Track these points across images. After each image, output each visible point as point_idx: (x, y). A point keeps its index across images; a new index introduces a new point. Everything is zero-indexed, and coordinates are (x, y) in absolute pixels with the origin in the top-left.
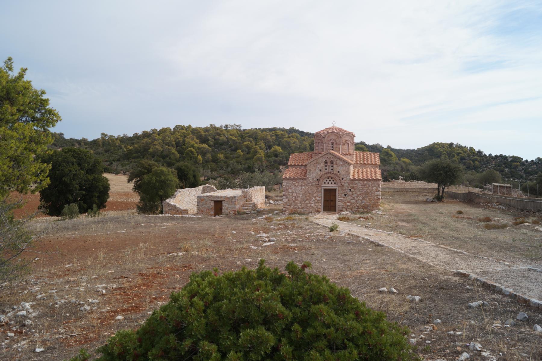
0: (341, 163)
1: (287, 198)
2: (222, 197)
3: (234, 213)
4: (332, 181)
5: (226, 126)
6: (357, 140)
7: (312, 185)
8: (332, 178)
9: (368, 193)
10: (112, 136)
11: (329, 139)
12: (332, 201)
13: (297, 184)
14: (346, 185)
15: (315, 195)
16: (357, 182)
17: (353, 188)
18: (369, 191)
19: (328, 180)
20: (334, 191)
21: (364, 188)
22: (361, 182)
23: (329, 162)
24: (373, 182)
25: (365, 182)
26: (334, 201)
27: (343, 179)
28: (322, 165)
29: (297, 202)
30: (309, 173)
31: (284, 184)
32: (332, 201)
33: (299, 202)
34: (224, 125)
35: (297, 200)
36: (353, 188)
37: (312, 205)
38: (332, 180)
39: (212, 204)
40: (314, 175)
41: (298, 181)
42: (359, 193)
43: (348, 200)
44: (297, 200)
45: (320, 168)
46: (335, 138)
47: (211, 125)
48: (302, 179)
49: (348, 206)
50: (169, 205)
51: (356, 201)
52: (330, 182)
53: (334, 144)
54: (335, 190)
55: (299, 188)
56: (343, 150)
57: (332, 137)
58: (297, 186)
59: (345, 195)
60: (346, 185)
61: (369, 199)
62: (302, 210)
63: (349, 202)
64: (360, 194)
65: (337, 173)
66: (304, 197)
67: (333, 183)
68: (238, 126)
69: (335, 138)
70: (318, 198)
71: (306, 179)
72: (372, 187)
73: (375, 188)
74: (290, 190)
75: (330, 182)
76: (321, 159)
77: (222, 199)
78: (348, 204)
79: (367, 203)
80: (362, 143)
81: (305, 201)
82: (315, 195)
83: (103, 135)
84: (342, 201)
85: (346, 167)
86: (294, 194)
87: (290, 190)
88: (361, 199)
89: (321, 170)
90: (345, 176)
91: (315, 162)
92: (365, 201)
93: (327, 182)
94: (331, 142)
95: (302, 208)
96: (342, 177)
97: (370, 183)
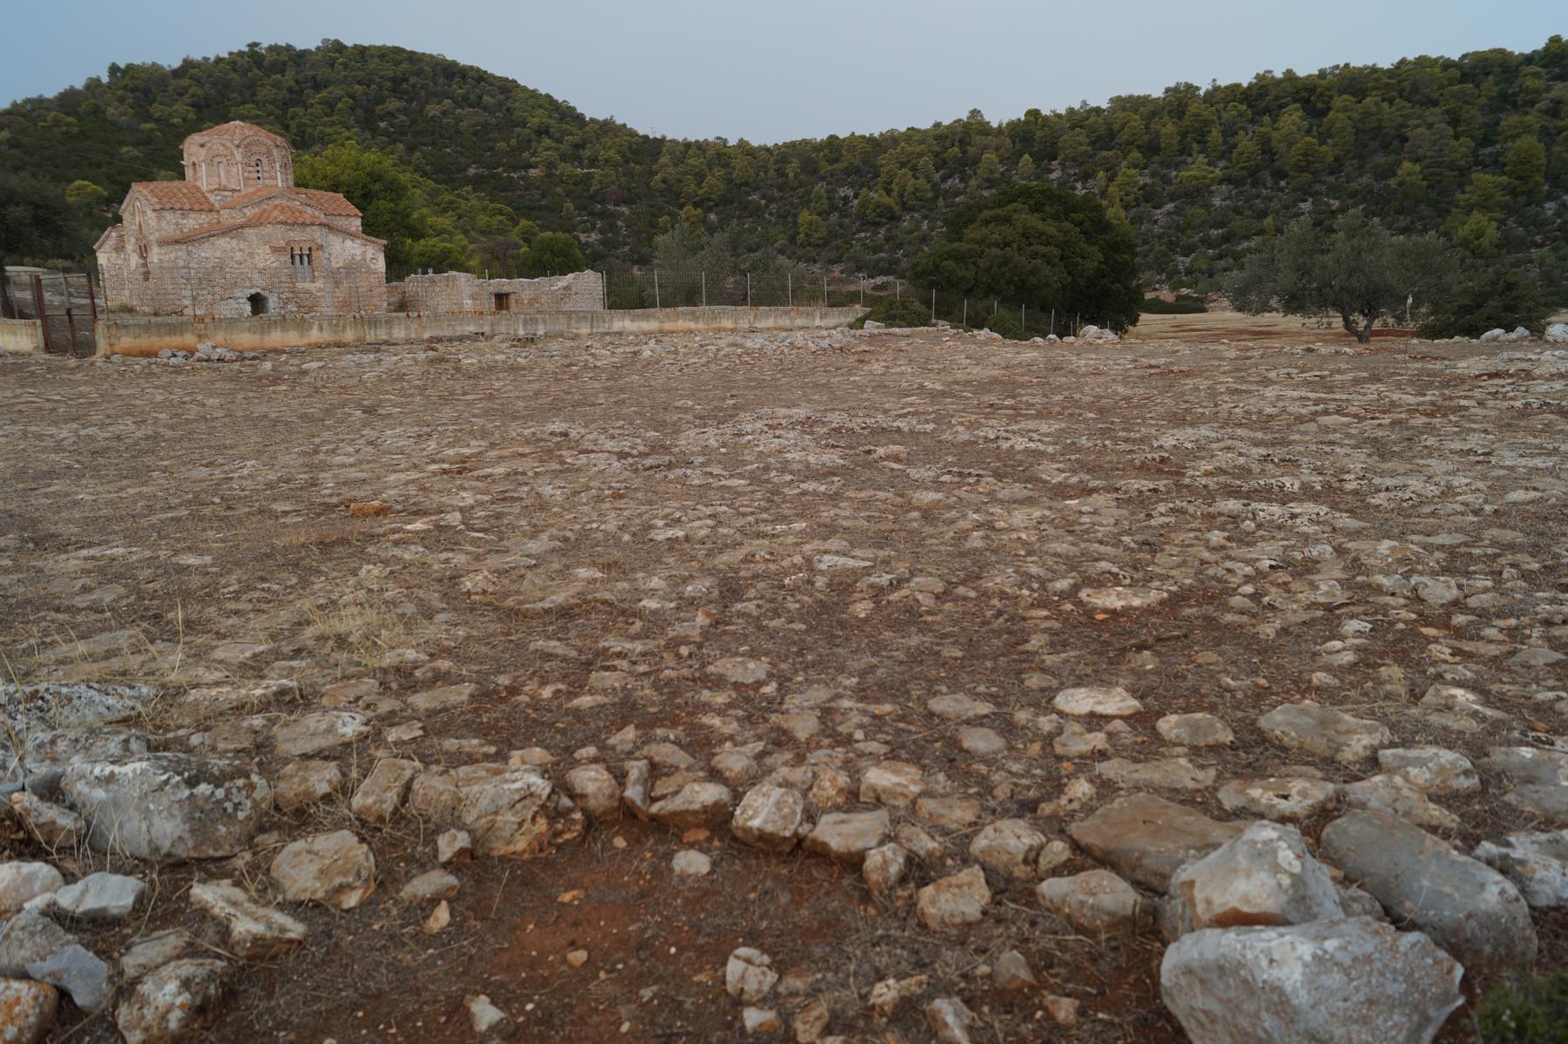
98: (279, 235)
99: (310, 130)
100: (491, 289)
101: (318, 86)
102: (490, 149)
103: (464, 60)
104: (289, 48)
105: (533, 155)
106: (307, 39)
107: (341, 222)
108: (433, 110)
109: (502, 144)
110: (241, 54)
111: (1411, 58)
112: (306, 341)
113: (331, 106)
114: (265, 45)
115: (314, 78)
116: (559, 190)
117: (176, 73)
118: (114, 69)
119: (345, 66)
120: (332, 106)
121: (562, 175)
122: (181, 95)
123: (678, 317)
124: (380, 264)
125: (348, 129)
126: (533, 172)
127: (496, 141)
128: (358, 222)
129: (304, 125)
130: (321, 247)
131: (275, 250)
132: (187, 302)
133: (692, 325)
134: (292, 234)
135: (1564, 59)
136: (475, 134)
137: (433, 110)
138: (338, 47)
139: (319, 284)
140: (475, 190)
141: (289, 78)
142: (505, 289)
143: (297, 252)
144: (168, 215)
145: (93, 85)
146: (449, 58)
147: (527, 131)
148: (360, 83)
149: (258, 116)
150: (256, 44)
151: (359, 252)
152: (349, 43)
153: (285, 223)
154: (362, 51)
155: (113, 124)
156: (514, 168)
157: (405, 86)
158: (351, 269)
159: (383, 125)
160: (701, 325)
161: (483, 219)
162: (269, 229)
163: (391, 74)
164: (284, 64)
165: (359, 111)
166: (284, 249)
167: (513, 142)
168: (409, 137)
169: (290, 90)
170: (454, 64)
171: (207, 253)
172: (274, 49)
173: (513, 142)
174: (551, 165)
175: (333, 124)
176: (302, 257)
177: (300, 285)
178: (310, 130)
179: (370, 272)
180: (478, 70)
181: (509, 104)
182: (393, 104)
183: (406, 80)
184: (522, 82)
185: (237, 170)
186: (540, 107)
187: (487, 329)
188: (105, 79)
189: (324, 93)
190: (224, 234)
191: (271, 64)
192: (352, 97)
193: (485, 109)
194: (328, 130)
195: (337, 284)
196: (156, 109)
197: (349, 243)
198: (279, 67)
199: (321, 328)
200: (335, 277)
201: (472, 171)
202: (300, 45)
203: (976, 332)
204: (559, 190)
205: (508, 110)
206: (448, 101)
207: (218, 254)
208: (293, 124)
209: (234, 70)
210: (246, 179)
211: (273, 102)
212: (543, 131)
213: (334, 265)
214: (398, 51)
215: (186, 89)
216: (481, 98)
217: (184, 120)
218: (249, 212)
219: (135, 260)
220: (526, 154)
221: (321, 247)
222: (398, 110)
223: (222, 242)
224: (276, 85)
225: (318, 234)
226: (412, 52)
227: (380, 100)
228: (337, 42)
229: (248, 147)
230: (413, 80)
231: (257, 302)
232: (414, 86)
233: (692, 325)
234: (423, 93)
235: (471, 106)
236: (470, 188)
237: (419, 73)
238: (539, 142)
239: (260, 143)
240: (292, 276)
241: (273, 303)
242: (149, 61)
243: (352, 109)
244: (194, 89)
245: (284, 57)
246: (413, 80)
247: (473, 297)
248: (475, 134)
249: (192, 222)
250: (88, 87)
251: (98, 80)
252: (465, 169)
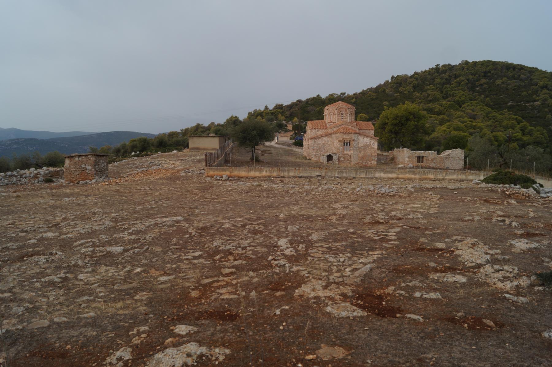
98: (340, 136)
99: (449, 92)
100: (416, 155)
101: (456, 77)
102: (519, 95)
103: (516, 62)
104: (449, 65)
105: (538, 96)
106: (456, 61)
107: (367, 132)
108: (498, 82)
109: (525, 93)
110: (433, 68)
111: (304, 99)
112: (261, 175)
113: (459, 83)
114: (441, 65)
115: (455, 74)
116: (546, 110)
117: (411, 77)
118: (393, 77)
119: (468, 69)
120: (460, 84)
121: (549, 103)
122: (410, 84)
123: (406, 173)
124: (376, 146)
125: (464, 91)
126: (536, 103)
127: (523, 92)
128: (373, 132)
129: (448, 91)
130: (354, 140)
131: (339, 141)
132: (312, 156)
133: (413, 176)
134: (345, 136)
135: (550, 72)
136: (514, 90)
137: (498, 82)
138: (467, 63)
139: (352, 152)
140: (509, 111)
141: (446, 75)
142: (422, 155)
143: (346, 142)
144: (314, 131)
145: (387, 83)
146: (510, 62)
147: (536, 87)
148: (472, 75)
149: (433, 89)
150: (438, 65)
151: (368, 142)
152: (471, 61)
153: (342, 133)
154: (475, 63)
155: (387, 94)
156: (528, 102)
157: (489, 74)
158: (365, 147)
159: (477, 89)
160: (417, 176)
161: (505, 122)
162: (338, 135)
163: (484, 70)
164: (446, 70)
165: (469, 84)
166: (341, 141)
167: (530, 92)
168: (487, 93)
169: (446, 79)
170: (511, 64)
171: (320, 142)
172: (444, 66)
173: (530, 92)
174: (545, 100)
175: (459, 90)
176: (347, 144)
177: (345, 152)
178: (449, 92)
179: (372, 148)
180: (521, 65)
181: (532, 77)
182: (483, 81)
183: (490, 72)
184: (540, 68)
185: (335, 116)
186: (545, 77)
187: (323, 174)
188: (390, 81)
189: (458, 79)
190: (326, 136)
191: (442, 71)
192: (468, 80)
193: (521, 80)
194: (456, 92)
195: (360, 152)
196: (401, 89)
197: (365, 139)
198: (444, 72)
199: (266, 171)
200: (359, 150)
201: (510, 104)
202: (453, 64)
203: (512, 185)
204: (546, 110)
205: (531, 79)
206: (505, 78)
207: (324, 142)
208: (444, 90)
209: (429, 74)
210: (338, 119)
211: (439, 84)
212: (545, 87)
213: (360, 146)
214: (489, 62)
215: (412, 82)
216: (520, 76)
217: (409, 92)
218: (335, 129)
220: (535, 96)
221: (354, 140)
222: (485, 83)
223: (325, 139)
224: (442, 78)
225: (353, 136)
226: (495, 62)
227: (478, 80)
228: (466, 61)
229: (339, 109)
230: (492, 72)
231: (330, 158)
232: (493, 74)
233: (413, 176)
234: (496, 76)
235: (515, 79)
236: (506, 110)
237: (495, 69)
238: (541, 91)
239: (343, 108)
240: (343, 149)
241: (335, 158)
242: (404, 74)
243: (467, 84)
244: (415, 82)
245: (446, 68)
246: (492, 72)
247: (409, 157)
248: (514, 90)
249: (320, 133)
250: (385, 83)
251: (388, 81)
252: (507, 103)
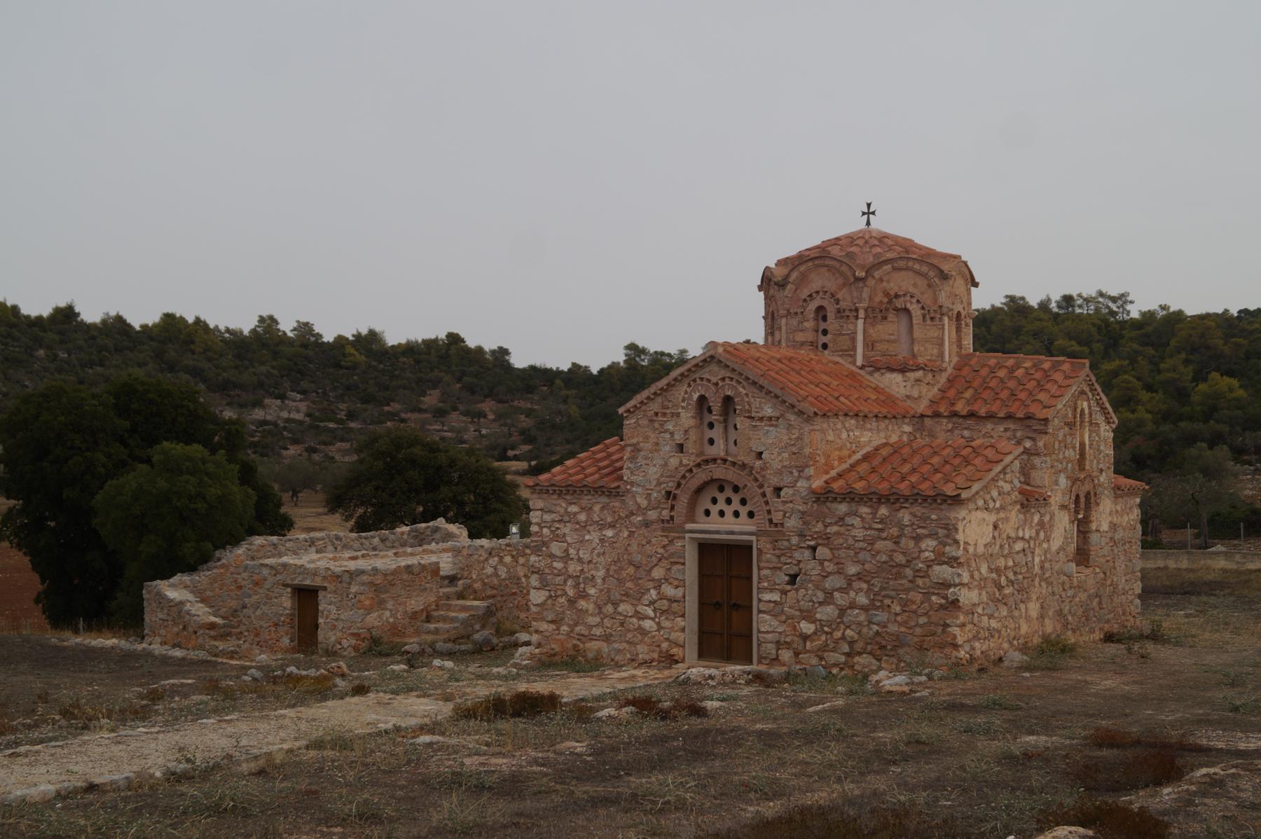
0: (768, 411)
1: (544, 585)
2: (315, 573)
3: (356, 648)
4: (736, 505)
5: (1068, 300)
6: (985, 298)
7: (647, 524)
8: (736, 489)
9: (896, 570)
10: (662, 354)
11: (804, 293)
12: (736, 606)
13: (582, 517)
14: (792, 523)
15: (657, 573)
16: (843, 508)
17: (826, 539)
18: (900, 558)
19: (721, 498)
20: (744, 550)
21: (880, 545)
22: (864, 510)
23: (716, 406)
24: (918, 510)
25: (883, 511)
26: (745, 608)
27: (778, 490)
28: (687, 418)
29: (582, 604)
30: (633, 459)
31: (535, 517)
32: (718, 605)
33: (591, 607)
34: (1056, 297)
35: (584, 595)
36: (826, 539)
37: (648, 624)
38: (736, 499)
39: (286, 602)
40: (653, 472)
41: (586, 500)
42: (852, 570)
43: (805, 605)
44: (584, 595)
45: (679, 438)
46: (831, 283)
47: (1012, 299)
48: (599, 490)
49: (805, 638)
50: (161, 596)
51: (842, 611)
52: (729, 510)
53: (831, 315)
54: (746, 549)
55: (593, 536)
56: (870, 345)
57: (819, 280)
58: (584, 527)
59: (793, 579)
60: (792, 523)
61: (905, 604)
62: (604, 647)
63: (808, 616)
64: (859, 577)
65: (749, 460)
66: (612, 582)
67: (743, 511)
68: (1114, 299)
69: (831, 283)
70: (669, 591)
71: (615, 493)
72: (918, 539)
73: (930, 544)
74: (556, 548)
75: (729, 510)
76: (681, 390)
77: (318, 582)
78: (807, 627)
79: (893, 628)
80: (1016, 306)
81: (615, 604)
82: (657, 573)
83: (634, 350)
84: (776, 610)
85: (790, 427)
86: (573, 568)
87: (556, 548)
88: (863, 600)
89: (681, 448)
90: (787, 479)
91: (655, 406)
92: (882, 616)
93: (714, 510)
94: (813, 306)
95: (607, 638)
96: (775, 481)
97: (905, 517)
219: (1063, 523)
